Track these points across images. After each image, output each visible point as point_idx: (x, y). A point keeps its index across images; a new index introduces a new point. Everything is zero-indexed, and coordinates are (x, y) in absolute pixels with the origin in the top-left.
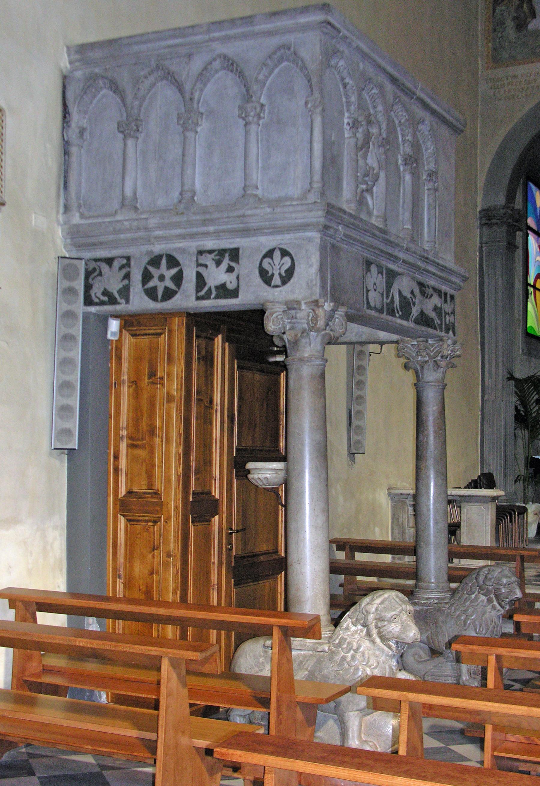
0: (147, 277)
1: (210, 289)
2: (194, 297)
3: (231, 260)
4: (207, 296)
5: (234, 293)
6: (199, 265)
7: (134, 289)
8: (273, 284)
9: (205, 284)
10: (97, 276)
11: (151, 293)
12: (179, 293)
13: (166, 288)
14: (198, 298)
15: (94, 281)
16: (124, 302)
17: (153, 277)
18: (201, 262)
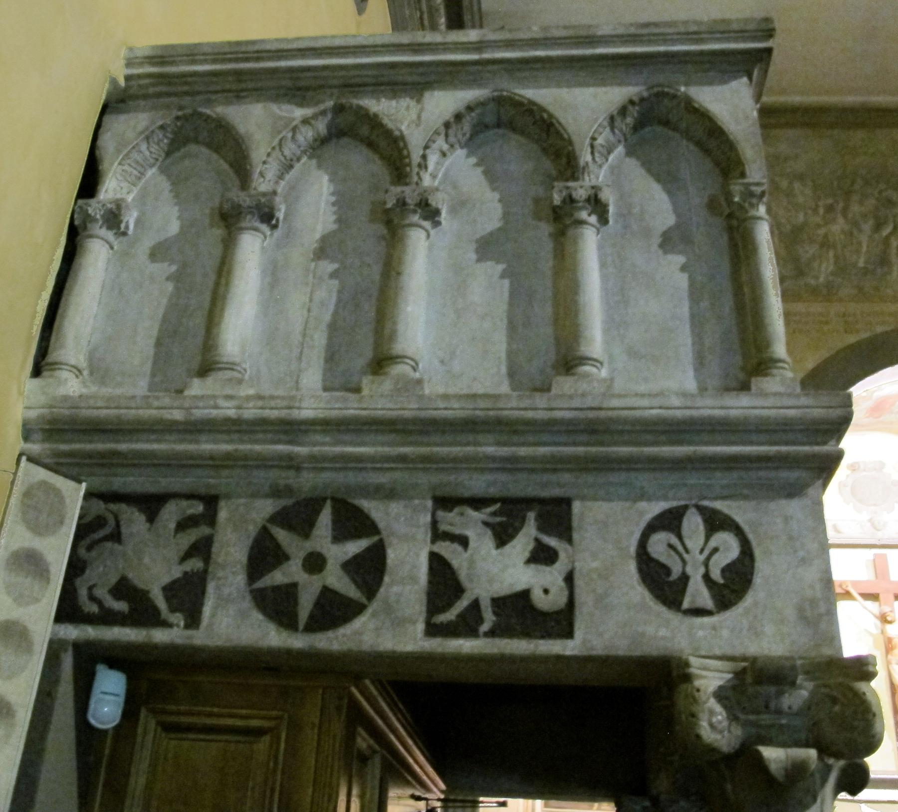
0: (264, 555)
1: (475, 605)
2: (421, 627)
3: (541, 529)
4: (468, 625)
5: (562, 622)
6: (438, 535)
7: (218, 588)
8: (686, 605)
9: (458, 590)
10: (106, 538)
11: (278, 605)
12: (370, 610)
13: (326, 591)
14: (433, 630)
15: (94, 553)
16: (182, 624)
17: (287, 558)
18: (443, 527)
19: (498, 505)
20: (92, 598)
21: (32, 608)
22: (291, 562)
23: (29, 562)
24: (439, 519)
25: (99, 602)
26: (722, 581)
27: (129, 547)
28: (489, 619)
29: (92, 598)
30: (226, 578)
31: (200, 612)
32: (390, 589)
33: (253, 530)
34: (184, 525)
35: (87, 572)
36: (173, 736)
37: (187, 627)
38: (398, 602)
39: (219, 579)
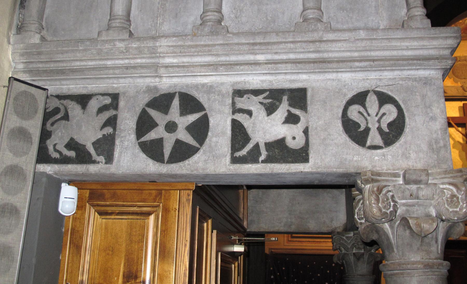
1: (257, 146)
3: (290, 105)
4: (253, 157)
5: (302, 155)
6: (236, 111)
8: (368, 143)
9: (247, 139)
11: (153, 150)
12: (201, 151)
13: (178, 142)
14: (235, 160)
15: (55, 126)
17: (156, 125)
19: (268, 93)
20: (56, 150)
21: (24, 158)
22: (159, 127)
23: (21, 134)
24: (236, 101)
25: (60, 153)
26: (388, 131)
27: (73, 121)
28: (264, 155)
29: (56, 150)
30: (125, 136)
31: (113, 155)
32: (211, 138)
33: (139, 110)
34: (101, 110)
35: (53, 136)
36: (103, 217)
37: (106, 163)
38: (216, 146)
39: (122, 137)
